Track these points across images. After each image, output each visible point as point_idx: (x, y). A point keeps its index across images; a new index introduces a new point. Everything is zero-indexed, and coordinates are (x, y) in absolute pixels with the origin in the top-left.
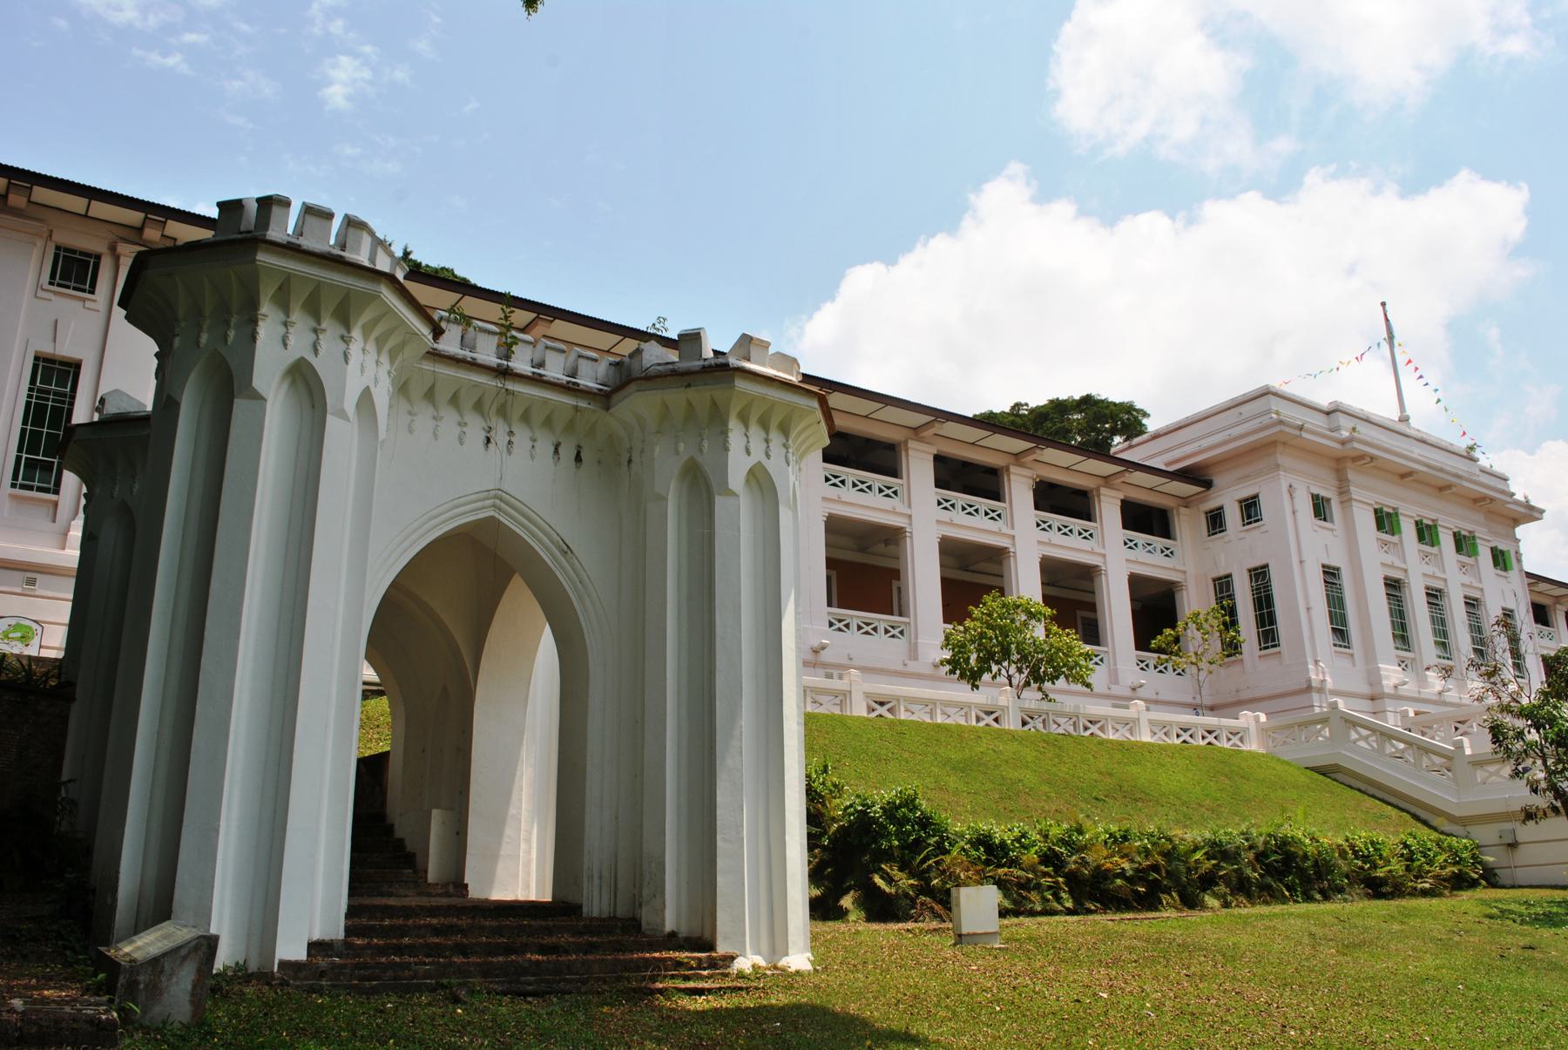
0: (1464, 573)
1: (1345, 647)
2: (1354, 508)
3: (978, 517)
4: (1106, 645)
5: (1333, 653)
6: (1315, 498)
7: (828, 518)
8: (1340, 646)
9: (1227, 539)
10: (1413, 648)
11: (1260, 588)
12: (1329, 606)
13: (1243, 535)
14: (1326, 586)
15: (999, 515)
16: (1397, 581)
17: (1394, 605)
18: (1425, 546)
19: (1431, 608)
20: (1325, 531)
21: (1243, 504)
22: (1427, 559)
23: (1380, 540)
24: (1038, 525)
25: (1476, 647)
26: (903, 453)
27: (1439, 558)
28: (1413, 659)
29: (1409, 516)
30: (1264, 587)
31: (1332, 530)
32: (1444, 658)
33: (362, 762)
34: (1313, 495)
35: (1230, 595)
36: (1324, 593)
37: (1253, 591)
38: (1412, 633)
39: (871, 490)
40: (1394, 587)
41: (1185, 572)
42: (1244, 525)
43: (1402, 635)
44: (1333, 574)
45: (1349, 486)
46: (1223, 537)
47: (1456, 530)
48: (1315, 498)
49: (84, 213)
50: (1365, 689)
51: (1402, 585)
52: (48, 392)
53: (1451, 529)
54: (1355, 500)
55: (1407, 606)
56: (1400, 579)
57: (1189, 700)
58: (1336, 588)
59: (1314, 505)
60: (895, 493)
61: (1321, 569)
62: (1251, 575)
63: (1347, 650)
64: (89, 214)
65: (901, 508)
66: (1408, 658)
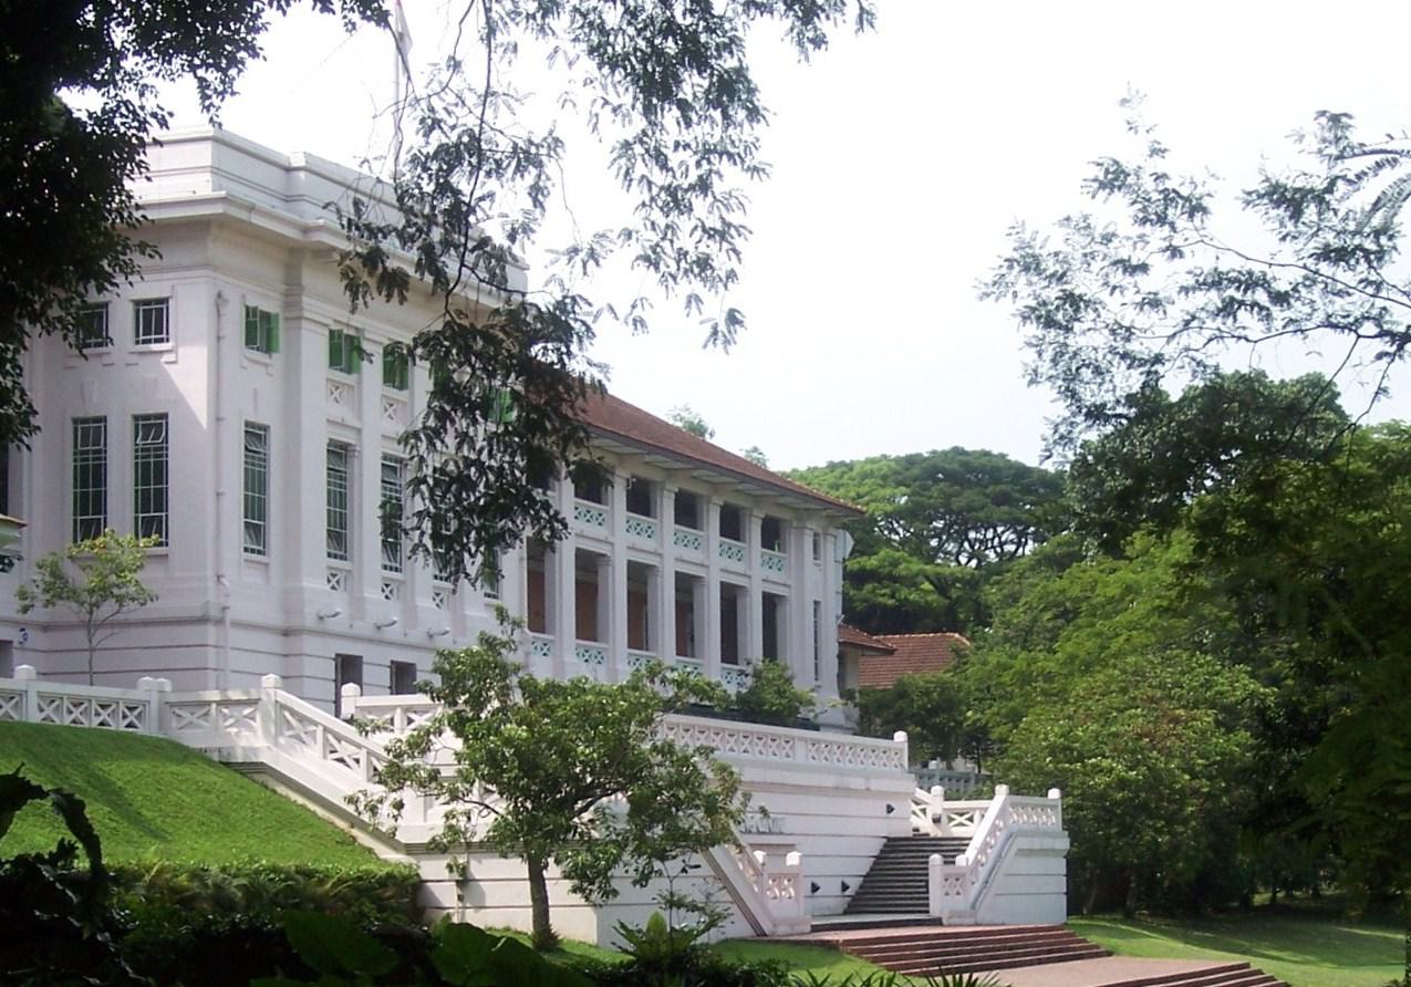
0: (390, 416)
1: (259, 552)
2: (303, 331)
4: (702, 657)
5: (243, 563)
6: (250, 312)
8: (253, 551)
9: (106, 360)
10: (352, 556)
11: (149, 450)
12: (246, 489)
13: (134, 359)
14: (246, 456)
16: (345, 447)
17: (335, 484)
18: (338, 373)
20: (256, 366)
21: (141, 308)
22: (391, 410)
23: (332, 381)
27: (356, 391)
28: (402, 583)
29: (375, 342)
30: (156, 449)
31: (266, 365)
32: (391, 569)
33: (864, 728)
34: (247, 308)
35: (99, 452)
36: (243, 466)
37: (137, 451)
38: (353, 533)
40: (339, 453)
42: (137, 343)
43: (338, 537)
44: (259, 437)
45: (300, 295)
46: (100, 355)
47: (335, 327)
48: (250, 312)
50: (274, 618)
51: (350, 454)
52: (87, 452)
53: (327, 325)
54: (306, 319)
55: (352, 486)
56: (350, 445)
57: (279, 651)
58: (260, 459)
59: (247, 323)
61: (243, 428)
62: (137, 427)
66: (341, 570)
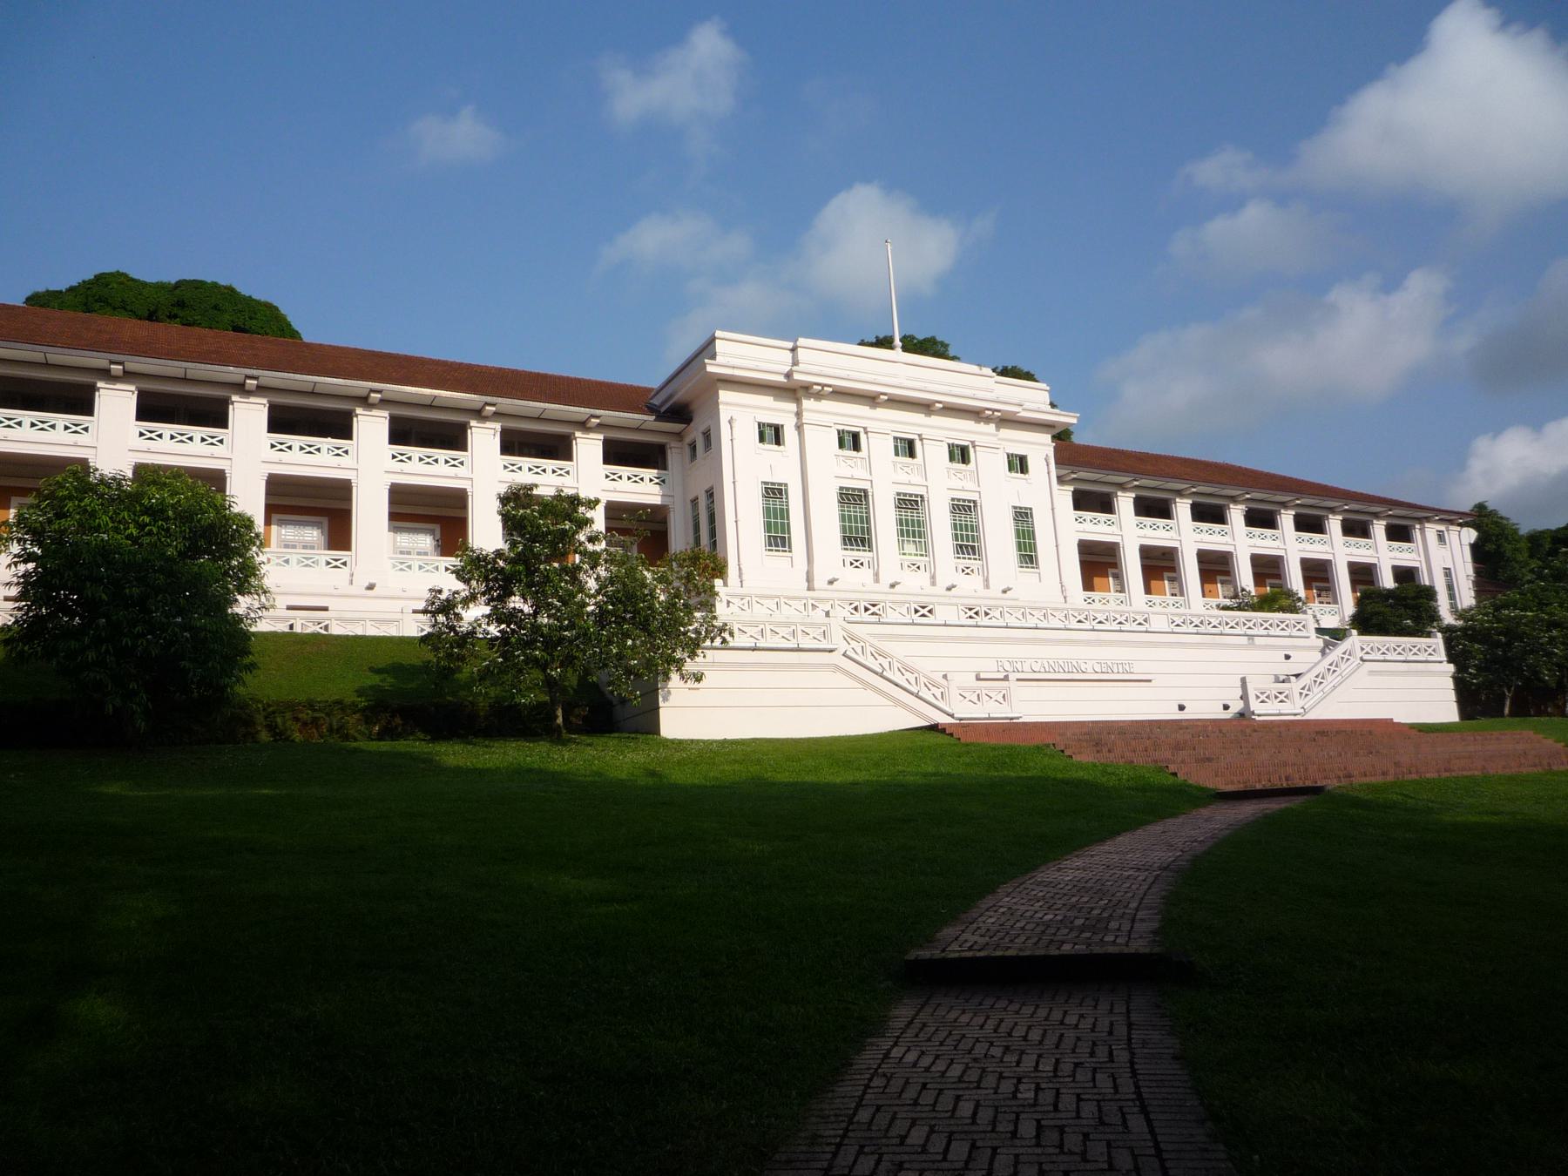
3: (1215, 536)
7: (135, 467)
15: (1113, 523)
19: (841, 506)
24: (1076, 520)
25: (1023, 553)
26: (1326, 522)
39: (319, 452)
41: (673, 496)
49: (183, 377)
60: (568, 473)
63: (1035, 570)
64: (187, 377)
65: (1231, 541)
